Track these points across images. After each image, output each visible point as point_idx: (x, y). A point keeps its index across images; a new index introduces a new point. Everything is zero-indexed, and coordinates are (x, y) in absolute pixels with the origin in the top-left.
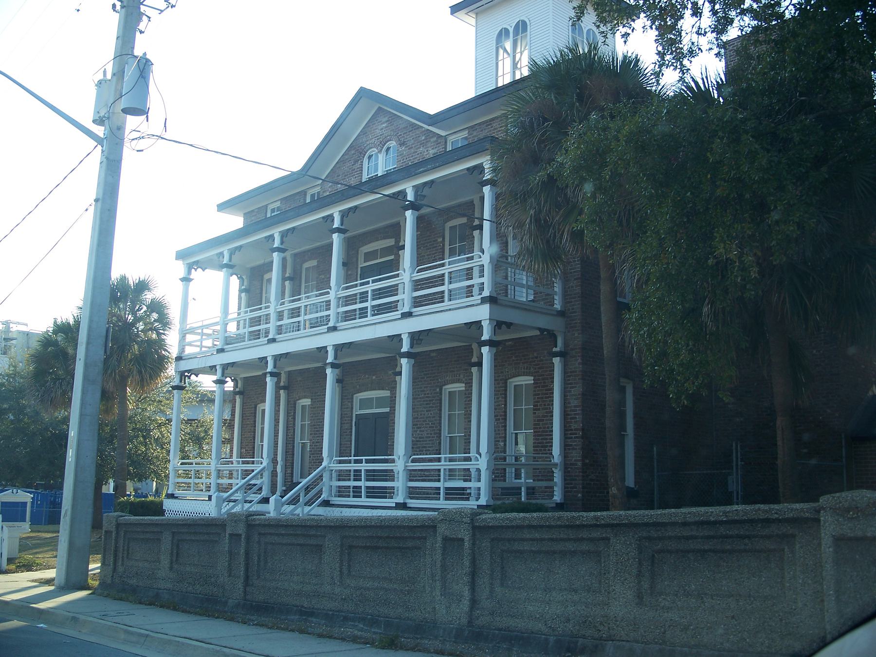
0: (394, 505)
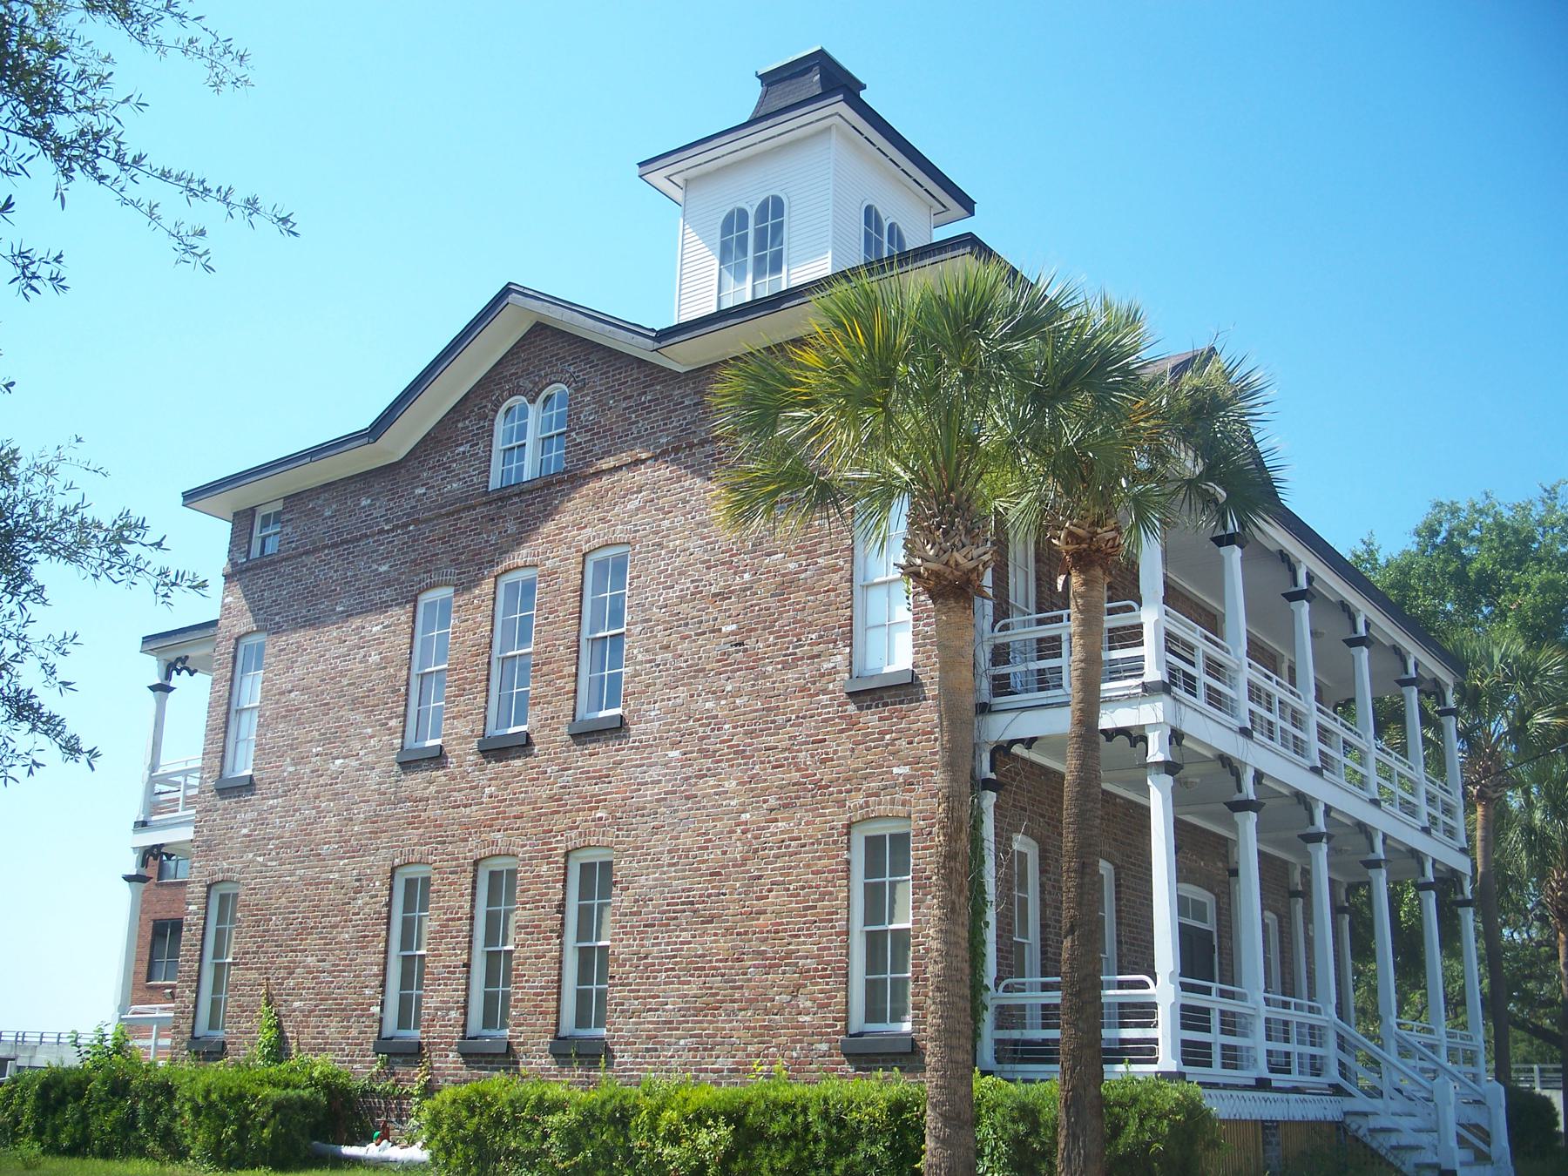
0: (1253, 1083)
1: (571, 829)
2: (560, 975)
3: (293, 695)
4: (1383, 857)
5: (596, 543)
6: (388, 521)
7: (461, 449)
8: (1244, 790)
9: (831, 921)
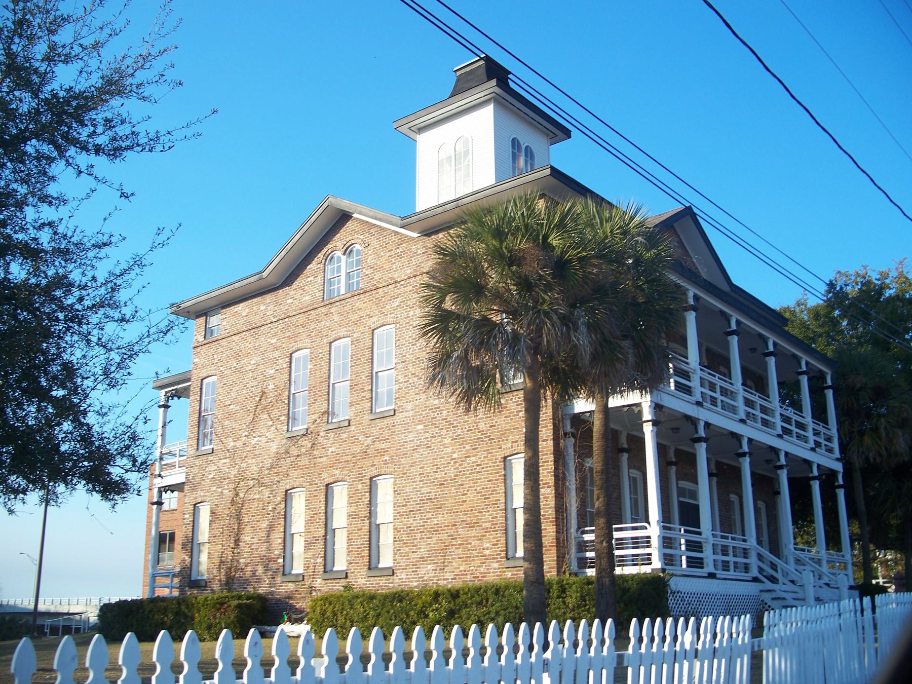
0: (706, 575)
1: (372, 466)
2: (370, 538)
3: (231, 407)
4: (785, 463)
5: (378, 324)
6: (275, 317)
7: (309, 279)
8: (699, 432)
9: (497, 504)
